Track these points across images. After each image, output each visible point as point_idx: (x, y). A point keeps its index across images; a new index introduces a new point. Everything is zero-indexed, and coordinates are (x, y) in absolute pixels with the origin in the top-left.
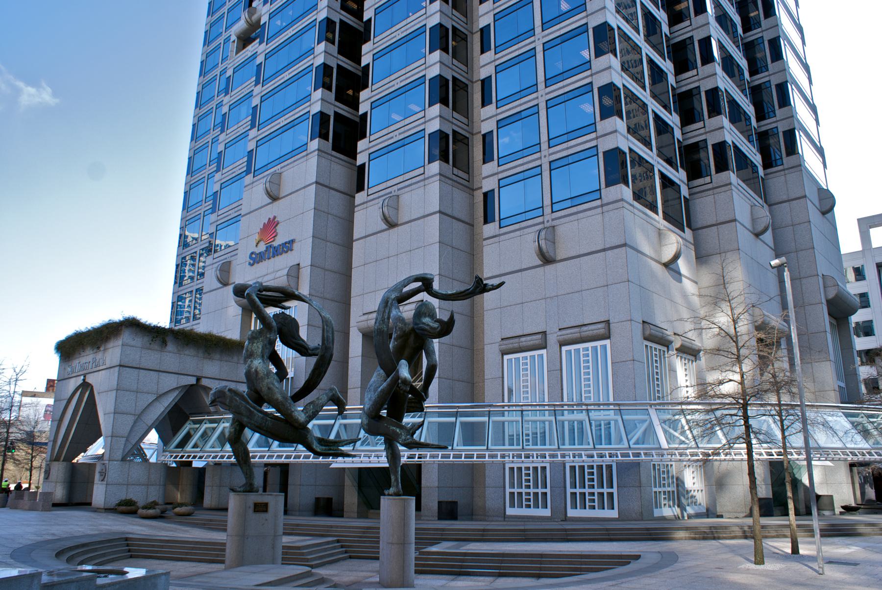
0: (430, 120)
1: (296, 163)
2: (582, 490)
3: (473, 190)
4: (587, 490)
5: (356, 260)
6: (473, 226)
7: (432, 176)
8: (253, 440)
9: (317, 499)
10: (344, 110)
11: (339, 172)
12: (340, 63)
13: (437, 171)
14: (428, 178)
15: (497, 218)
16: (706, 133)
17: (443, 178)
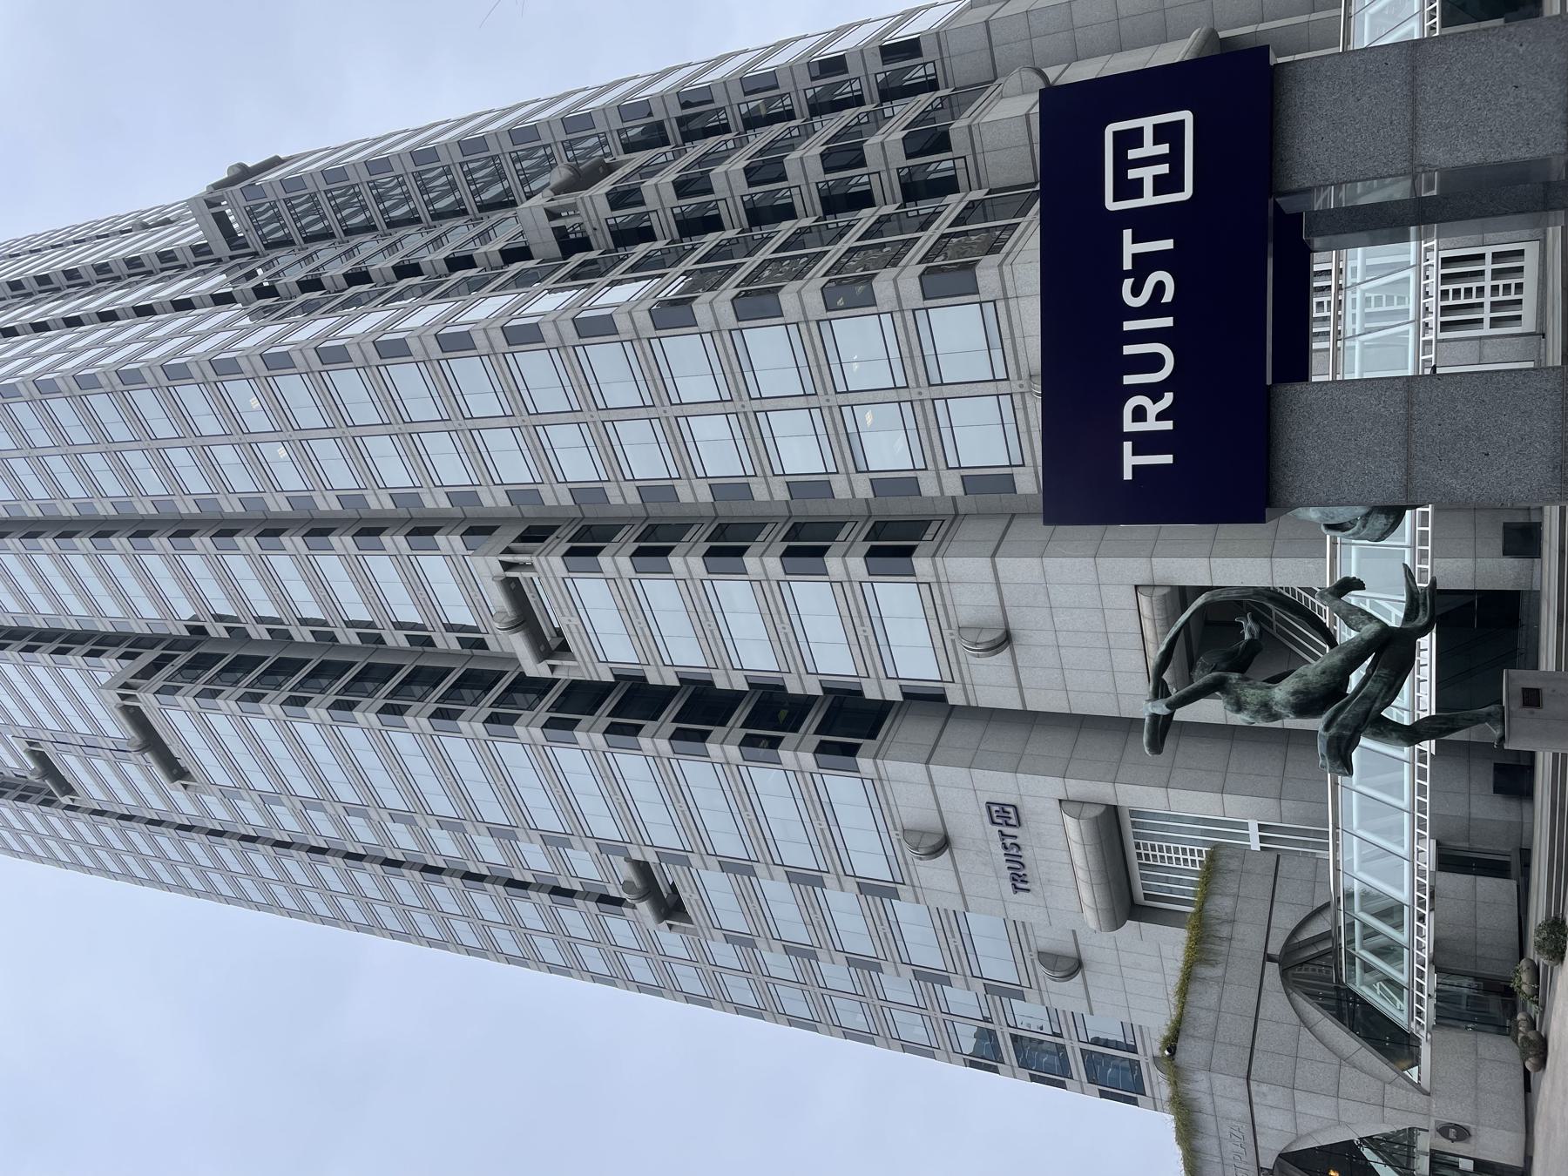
0: (848, 574)
1: (891, 802)
2: (1487, 307)
3: (957, 515)
4: (1487, 299)
5: (1057, 705)
6: (1013, 515)
7: (936, 569)
8: (1399, 712)
9: (1497, 790)
10: (813, 720)
11: (906, 732)
12: (740, 723)
13: (928, 561)
14: (937, 576)
15: (1007, 471)
16: (888, 170)
17: (940, 552)
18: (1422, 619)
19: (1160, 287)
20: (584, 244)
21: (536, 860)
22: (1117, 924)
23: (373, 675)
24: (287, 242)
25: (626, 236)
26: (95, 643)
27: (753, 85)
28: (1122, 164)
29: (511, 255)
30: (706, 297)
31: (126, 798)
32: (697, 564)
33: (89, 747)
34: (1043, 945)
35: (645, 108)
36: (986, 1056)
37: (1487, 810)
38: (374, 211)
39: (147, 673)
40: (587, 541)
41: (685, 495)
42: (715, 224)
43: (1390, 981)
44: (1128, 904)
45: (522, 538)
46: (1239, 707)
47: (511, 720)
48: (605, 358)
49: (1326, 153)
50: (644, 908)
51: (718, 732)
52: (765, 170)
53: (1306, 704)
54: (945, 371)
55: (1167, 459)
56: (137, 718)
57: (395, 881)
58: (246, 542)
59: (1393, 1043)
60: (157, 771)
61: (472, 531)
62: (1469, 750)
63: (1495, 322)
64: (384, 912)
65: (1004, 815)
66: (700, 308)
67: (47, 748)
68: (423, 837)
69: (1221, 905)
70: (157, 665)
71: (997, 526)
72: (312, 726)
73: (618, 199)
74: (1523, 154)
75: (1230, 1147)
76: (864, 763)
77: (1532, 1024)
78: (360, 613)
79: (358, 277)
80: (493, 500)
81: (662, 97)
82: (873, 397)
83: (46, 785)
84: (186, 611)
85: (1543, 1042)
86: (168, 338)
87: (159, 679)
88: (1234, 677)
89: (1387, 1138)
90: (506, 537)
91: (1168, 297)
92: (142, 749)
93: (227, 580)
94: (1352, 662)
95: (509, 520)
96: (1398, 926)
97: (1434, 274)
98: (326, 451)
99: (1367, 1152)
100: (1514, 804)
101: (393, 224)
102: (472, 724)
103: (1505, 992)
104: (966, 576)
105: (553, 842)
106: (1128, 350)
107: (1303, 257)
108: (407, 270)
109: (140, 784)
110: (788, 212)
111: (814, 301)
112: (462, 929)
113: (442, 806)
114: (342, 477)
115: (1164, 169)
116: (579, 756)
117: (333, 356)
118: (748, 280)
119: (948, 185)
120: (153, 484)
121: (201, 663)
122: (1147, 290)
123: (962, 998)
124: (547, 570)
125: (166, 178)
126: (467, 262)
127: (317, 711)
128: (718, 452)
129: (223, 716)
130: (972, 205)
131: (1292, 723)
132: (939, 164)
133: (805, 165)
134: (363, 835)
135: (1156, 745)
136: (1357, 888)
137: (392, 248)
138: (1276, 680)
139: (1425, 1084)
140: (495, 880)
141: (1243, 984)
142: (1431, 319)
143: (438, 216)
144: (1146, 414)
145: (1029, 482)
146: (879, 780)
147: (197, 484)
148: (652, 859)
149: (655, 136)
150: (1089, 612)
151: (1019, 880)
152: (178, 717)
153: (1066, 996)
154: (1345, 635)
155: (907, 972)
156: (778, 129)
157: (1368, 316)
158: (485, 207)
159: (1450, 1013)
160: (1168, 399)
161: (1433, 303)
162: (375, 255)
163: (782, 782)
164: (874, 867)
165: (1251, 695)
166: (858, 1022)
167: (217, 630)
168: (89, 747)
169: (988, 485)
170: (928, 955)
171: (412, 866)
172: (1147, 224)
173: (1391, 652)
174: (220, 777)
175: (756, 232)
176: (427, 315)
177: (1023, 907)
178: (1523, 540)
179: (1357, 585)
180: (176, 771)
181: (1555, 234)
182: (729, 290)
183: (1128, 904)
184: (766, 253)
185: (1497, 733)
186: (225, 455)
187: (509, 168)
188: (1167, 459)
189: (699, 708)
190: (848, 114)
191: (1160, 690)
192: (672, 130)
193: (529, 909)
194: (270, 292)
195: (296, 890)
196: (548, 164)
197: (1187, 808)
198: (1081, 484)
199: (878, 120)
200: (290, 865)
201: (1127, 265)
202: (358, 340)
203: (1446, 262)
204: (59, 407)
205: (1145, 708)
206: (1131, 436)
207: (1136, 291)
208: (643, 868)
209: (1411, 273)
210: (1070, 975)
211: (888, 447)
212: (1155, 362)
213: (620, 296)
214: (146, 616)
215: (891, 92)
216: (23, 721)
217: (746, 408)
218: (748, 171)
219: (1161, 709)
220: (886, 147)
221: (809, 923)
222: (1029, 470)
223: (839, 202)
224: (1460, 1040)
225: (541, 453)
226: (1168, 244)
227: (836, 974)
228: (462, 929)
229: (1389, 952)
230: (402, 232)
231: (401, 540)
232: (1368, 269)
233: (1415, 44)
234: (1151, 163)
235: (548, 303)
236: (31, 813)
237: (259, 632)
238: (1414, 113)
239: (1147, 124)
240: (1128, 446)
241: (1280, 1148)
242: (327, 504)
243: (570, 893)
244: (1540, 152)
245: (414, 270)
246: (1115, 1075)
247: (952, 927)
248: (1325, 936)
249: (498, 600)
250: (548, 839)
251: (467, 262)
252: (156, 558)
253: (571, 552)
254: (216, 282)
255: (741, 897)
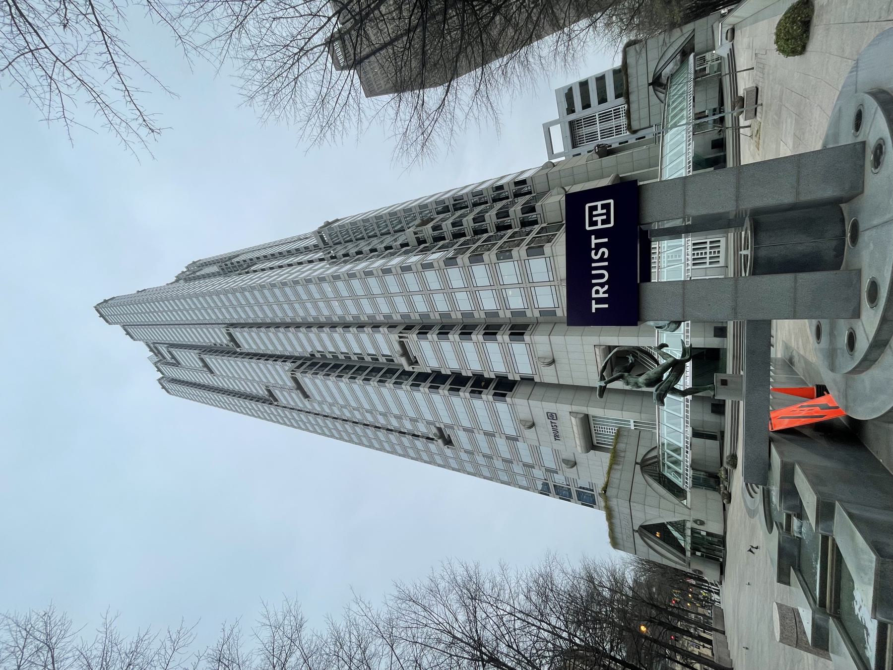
4: (708, 256)
8: (680, 386)
10: (492, 386)
11: (521, 390)
18: (687, 357)
19: (603, 253)
20: (425, 242)
21: (408, 426)
22: (588, 451)
23: (361, 369)
24: (340, 243)
25: (437, 239)
26: (285, 358)
27: (475, 194)
28: (608, 214)
29: (403, 245)
30: (461, 256)
31: (292, 403)
32: (457, 337)
33: (282, 388)
34: (564, 457)
35: (443, 202)
36: (545, 491)
37: (709, 418)
38: (364, 233)
39: (298, 367)
40: (424, 329)
41: (453, 316)
42: (464, 235)
43: (676, 472)
44: (591, 445)
45: (405, 329)
46: (628, 384)
47: (401, 383)
48: (430, 275)
49: (656, 213)
50: (440, 441)
51: (463, 389)
52: (479, 219)
53: (650, 384)
54: (538, 278)
55: (606, 306)
56: (296, 380)
57: (390, 436)
58: (326, 329)
59: (678, 492)
60: (301, 395)
61: (390, 327)
62: (703, 398)
63: (710, 263)
64: (363, 439)
65: (552, 416)
66: (459, 260)
67: (271, 388)
68: (374, 417)
69: (621, 446)
70: (301, 365)
71: (551, 326)
72: (344, 383)
73: (435, 228)
74: (721, 211)
75: (623, 523)
76: (508, 399)
77: (726, 488)
78: (358, 351)
79: (359, 253)
80: (397, 318)
81: (448, 198)
82: (512, 286)
83: (270, 399)
84: (309, 350)
85: (730, 494)
86: (307, 271)
87: (302, 369)
88: (626, 374)
89: (676, 522)
90: (400, 328)
91: (606, 256)
92: (297, 389)
93: (321, 341)
94: (665, 370)
95: (401, 324)
96: (679, 454)
97: (690, 248)
98: (365, 302)
99: (669, 527)
100: (718, 416)
101: (369, 237)
102: (389, 384)
103: (716, 478)
104: (540, 341)
105: (412, 420)
106: (594, 272)
107: (649, 243)
108: (373, 250)
109: (296, 399)
110: (486, 231)
111: (467, 261)
112: (398, 448)
113: (381, 408)
114: (353, 311)
115: (604, 217)
116: (422, 394)
117: (352, 276)
118: (473, 252)
119: (535, 222)
120: (301, 313)
121: (313, 365)
122: (600, 254)
123: (538, 473)
124: (412, 338)
125: (305, 224)
126: (391, 248)
127: (345, 379)
128: (464, 303)
129: (319, 380)
130: (542, 228)
131: (645, 389)
132: (532, 216)
133: (491, 217)
134: (358, 416)
135: (601, 395)
136: (666, 442)
137: (369, 244)
138: (640, 375)
139: (689, 506)
140: (396, 431)
141: (628, 471)
142: (689, 262)
143: (382, 234)
144: (601, 292)
145: (562, 312)
146: (513, 405)
147: (313, 313)
148: (442, 427)
149: (446, 210)
150: (582, 353)
151: (556, 437)
152: (307, 380)
153: (571, 473)
154: (662, 361)
155: (521, 464)
156: (483, 206)
157: (669, 261)
158: (396, 232)
159: (697, 483)
160: (606, 287)
161: (690, 257)
162: (364, 246)
163: (482, 405)
164: (511, 432)
165: (632, 380)
166: (505, 478)
167: (318, 355)
168: (282, 388)
169: (548, 314)
170: (528, 460)
171: (372, 426)
172: (599, 234)
173: (677, 367)
174: (318, 398)
175: (476, 237)
176: (379, 263)
177: (557, 445)
178: (721, 332)
179: (666, 346)
180: (306, 396)
181: (731, 236)
182: (468, 254)
183: (591, 445)
184: (505, 239)
185: (712, 393)
186: (321, 304)
187: (403, 220)
188: (606, 306)
189: (458, 381)
190: (504, 202)
191: (602, 378)
192: (451, 208)
193: (406, 440)
194: (334, 257)
195: (339, 432)
196: (414, 219)
197: (611, 415)
198: (579, 313)
199: (513, 203)
200: (337, 424)
201: (593, 246)
202: (359, 271)
203: (694, 244)
204: (276, 291)
205: (598, 384)
206: (594, 299)
207: (596, 254)
208: (440, 429)
209: (683, 248)
210: (572, 467)
211: (516, 302)
212: (602, 276)
213: (435, 257)
214: (298, 351)
215: (517, 195)
216: (264, 380)
217: (473, 290)
218: (473, 219)
219: (603, 384)
220: (516, 211)
221: (490, 448)
222: (560, 309)
223: (501, 228)
224: (701, 492)
225: (392, 305)
226: (606, 240)
227: (499, 464)
228: (398, 448)
229: (676, 463)
230: (372, 239)
231: (370, 329)
232: (669, 247)
233: (686, 178)
234: (600, 216)
235: (414, 259)
236: (266, 406)
237: (329, 356)
238: (685, 199)
239: (599, 204)
240: (594, 302)
241: (640, 524)
242: (335, 319)
243: (418, 436)
244: (727, 210)
245: (375, 250)
246: (586, 498)
247: (535, 450)
248: (655, 457)
249: (397, 347)
250: (411, 420)
251: (391, 248)
252: (302, 334)
253: (419, 333)
254: (320, 255)
255: (470, 439)
